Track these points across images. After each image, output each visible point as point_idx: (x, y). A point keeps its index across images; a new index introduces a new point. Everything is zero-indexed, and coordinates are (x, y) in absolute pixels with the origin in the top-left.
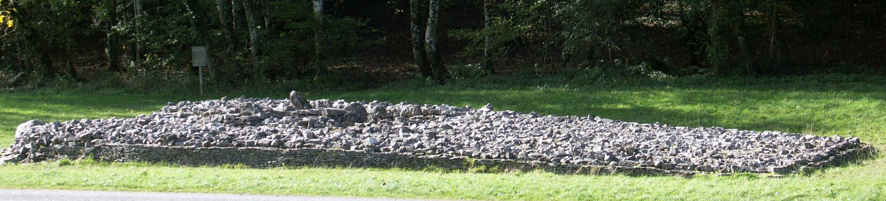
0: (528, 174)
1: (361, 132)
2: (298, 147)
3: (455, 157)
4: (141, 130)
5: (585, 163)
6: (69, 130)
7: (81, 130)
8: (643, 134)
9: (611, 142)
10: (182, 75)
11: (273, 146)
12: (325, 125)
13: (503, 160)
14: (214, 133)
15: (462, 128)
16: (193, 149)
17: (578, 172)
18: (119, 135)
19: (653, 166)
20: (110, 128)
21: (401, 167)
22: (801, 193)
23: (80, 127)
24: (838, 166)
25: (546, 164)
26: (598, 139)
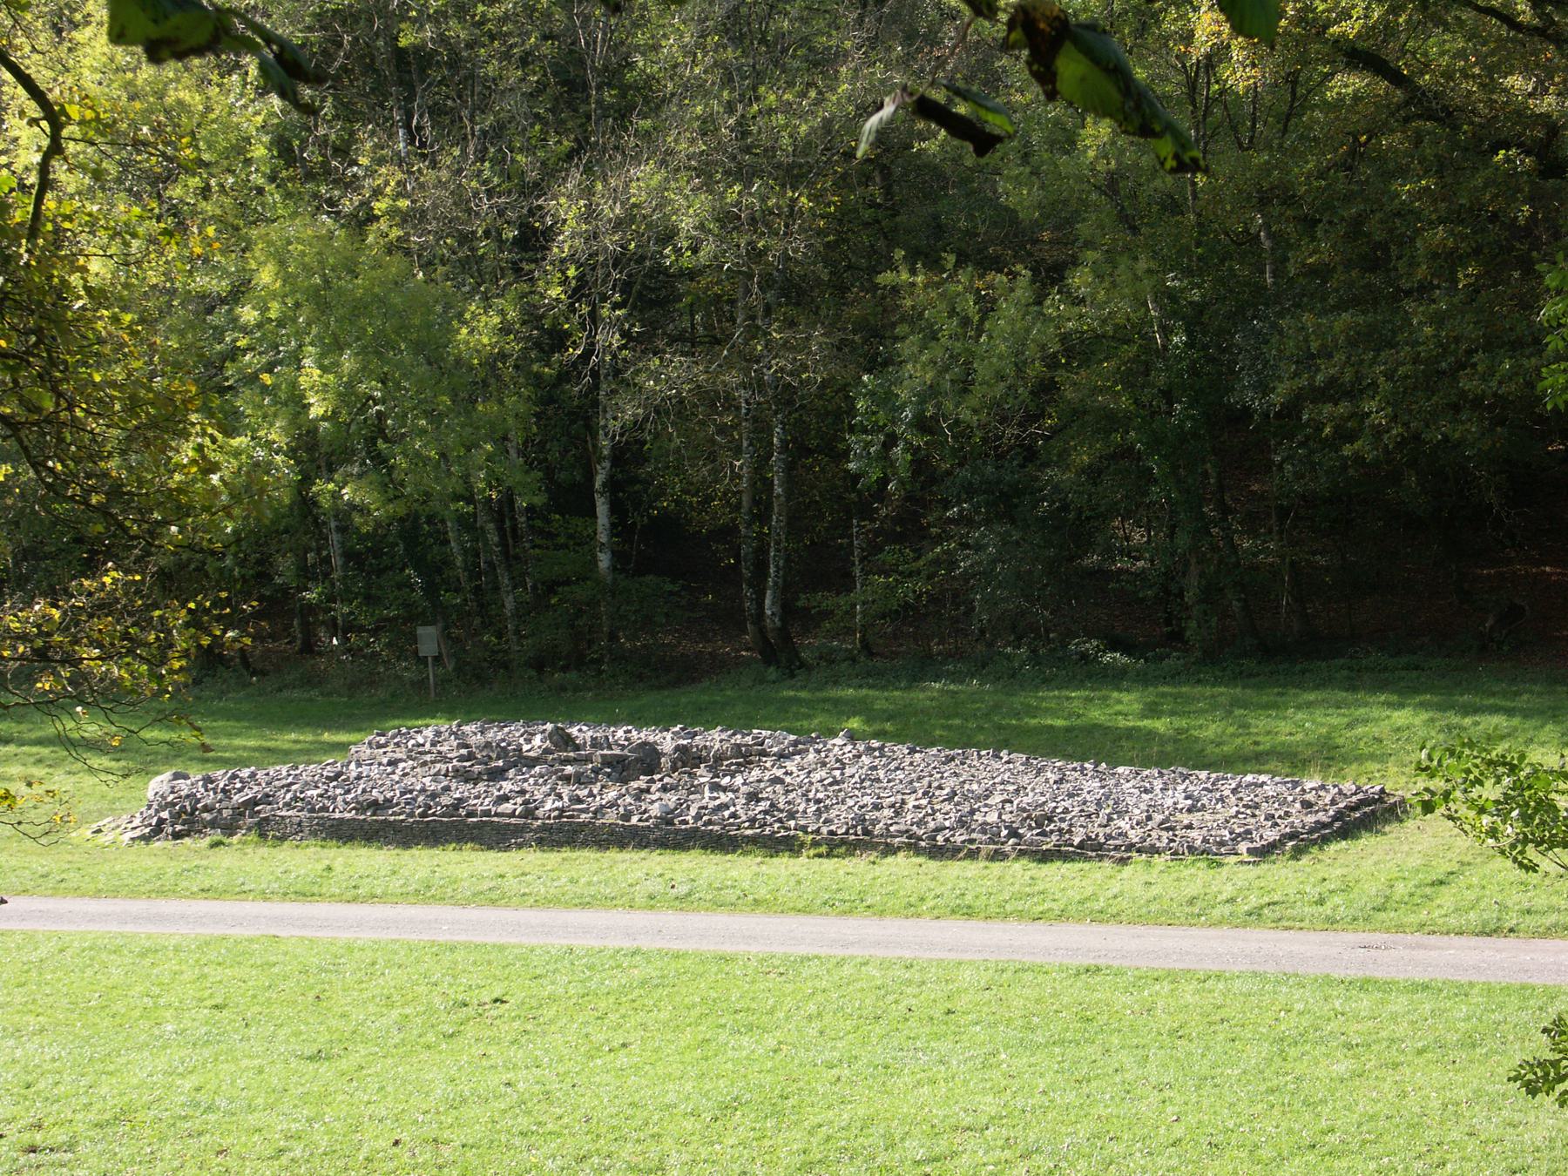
0: (890, 859)
1: (648, 791)
2: (555, 818)
3: (783, 833)
4: (327, 791)
5: (972, 841)
6: (224, 791)
7: (240, 790)
8: (1066, 786)
9: (1016, 803)
10: (406, 670)
11: (519, 816)
12: (597, 780)
13: (853, 837)
14: (434, 795)
15: (799, 780)
16: (402, 821)
17: (961, 855)
18: (295, 799)
19: (1072, 845)
20: (283, 787)
21: (704, 848)
22: (1276, 898)
23: (238, 785)
24: (1345, 839)
25: (916, 844)
26: (996, 799)
